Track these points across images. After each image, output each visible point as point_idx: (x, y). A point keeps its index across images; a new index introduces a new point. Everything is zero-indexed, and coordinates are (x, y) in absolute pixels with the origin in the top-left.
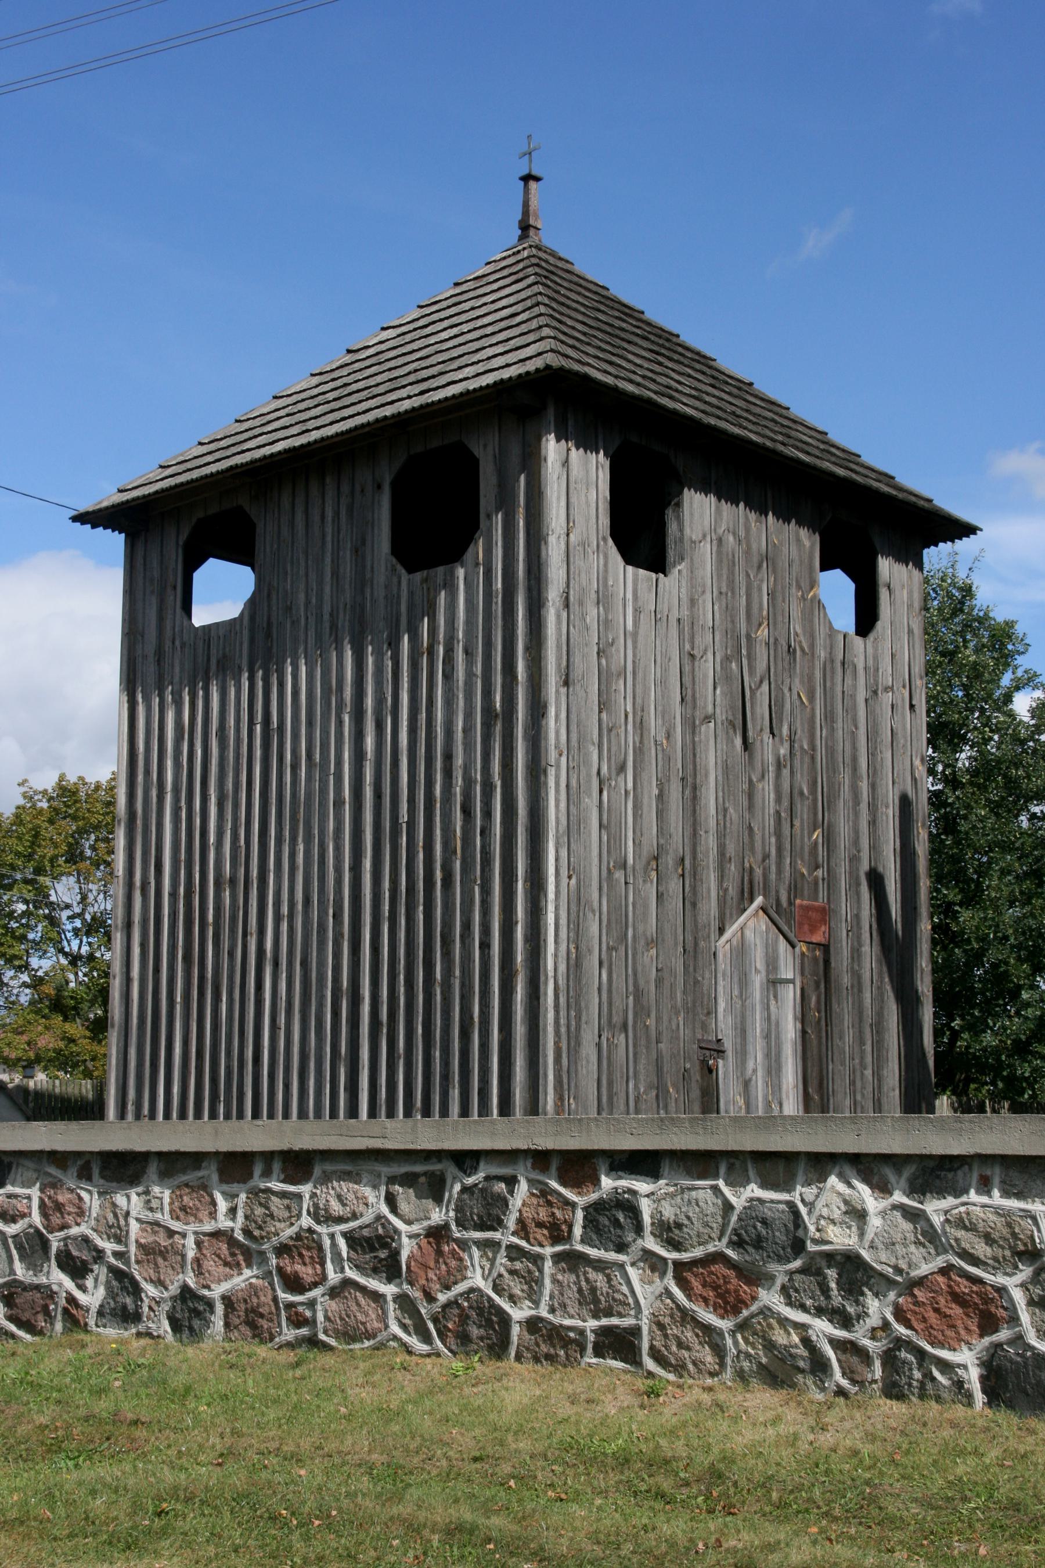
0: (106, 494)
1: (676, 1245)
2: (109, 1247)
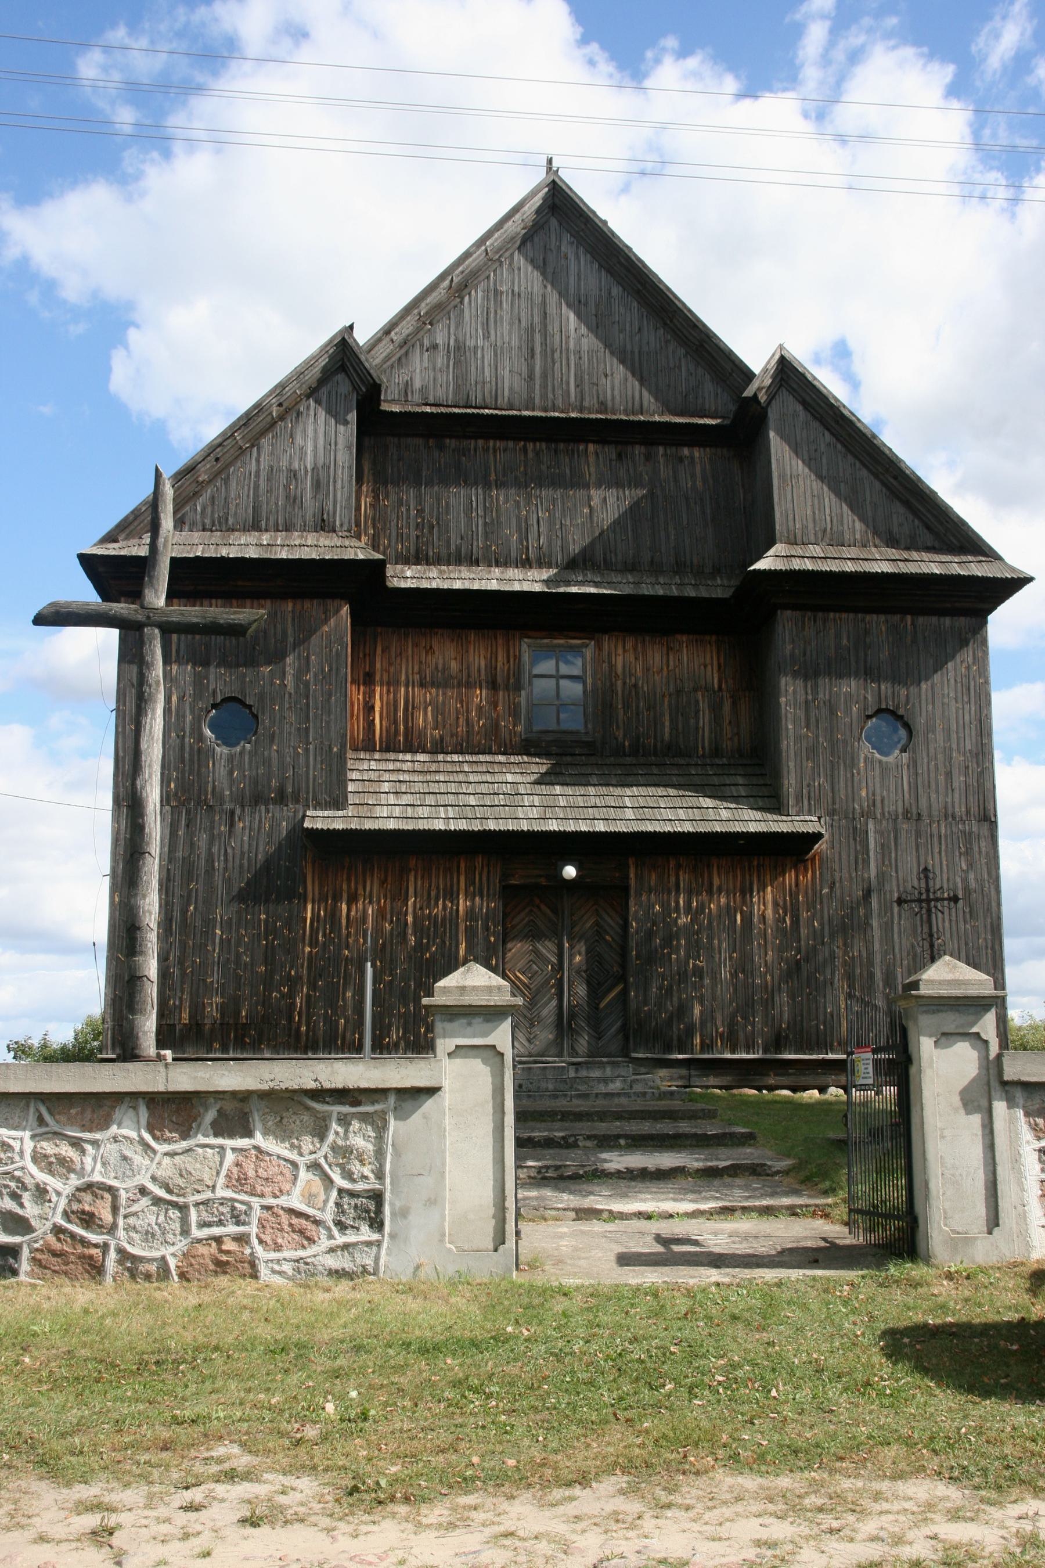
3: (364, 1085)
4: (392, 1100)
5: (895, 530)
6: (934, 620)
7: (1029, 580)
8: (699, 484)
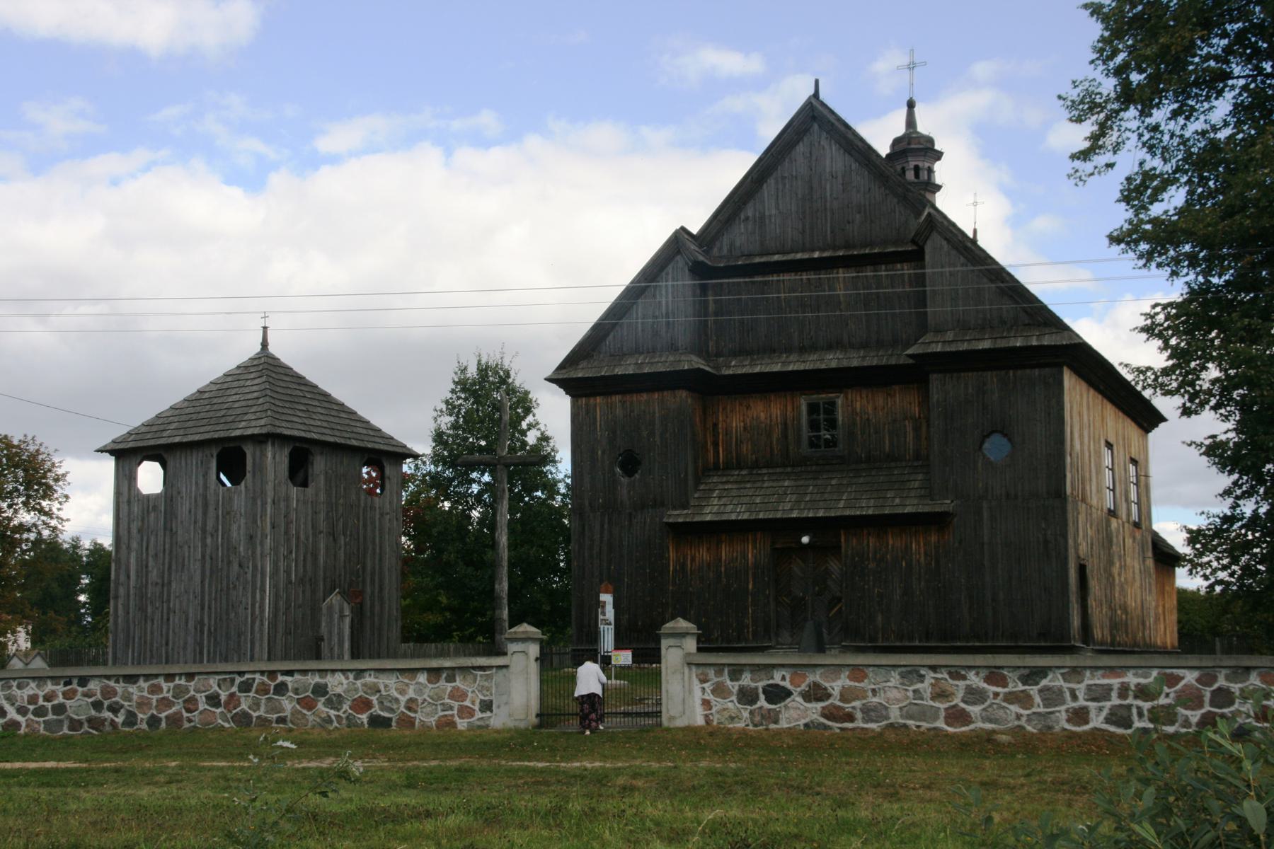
0: (106, 440)
1: (297, 694)
2: (126, 704)
6: (1028, 371)
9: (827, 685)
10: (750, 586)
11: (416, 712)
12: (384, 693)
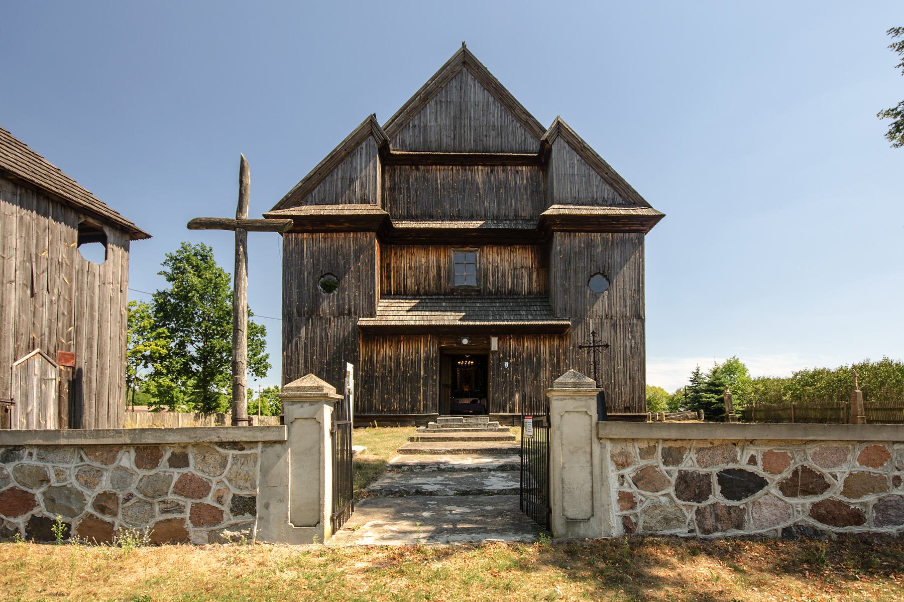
3: (244, 439)
4: (260, 446)
5: (606, 196)
6: (621, 235)
7: (664, 215)
8: (525, 182)
9: (825, 471)
10: (422, 373)
11: (115, 514)
12: (54, 482)
